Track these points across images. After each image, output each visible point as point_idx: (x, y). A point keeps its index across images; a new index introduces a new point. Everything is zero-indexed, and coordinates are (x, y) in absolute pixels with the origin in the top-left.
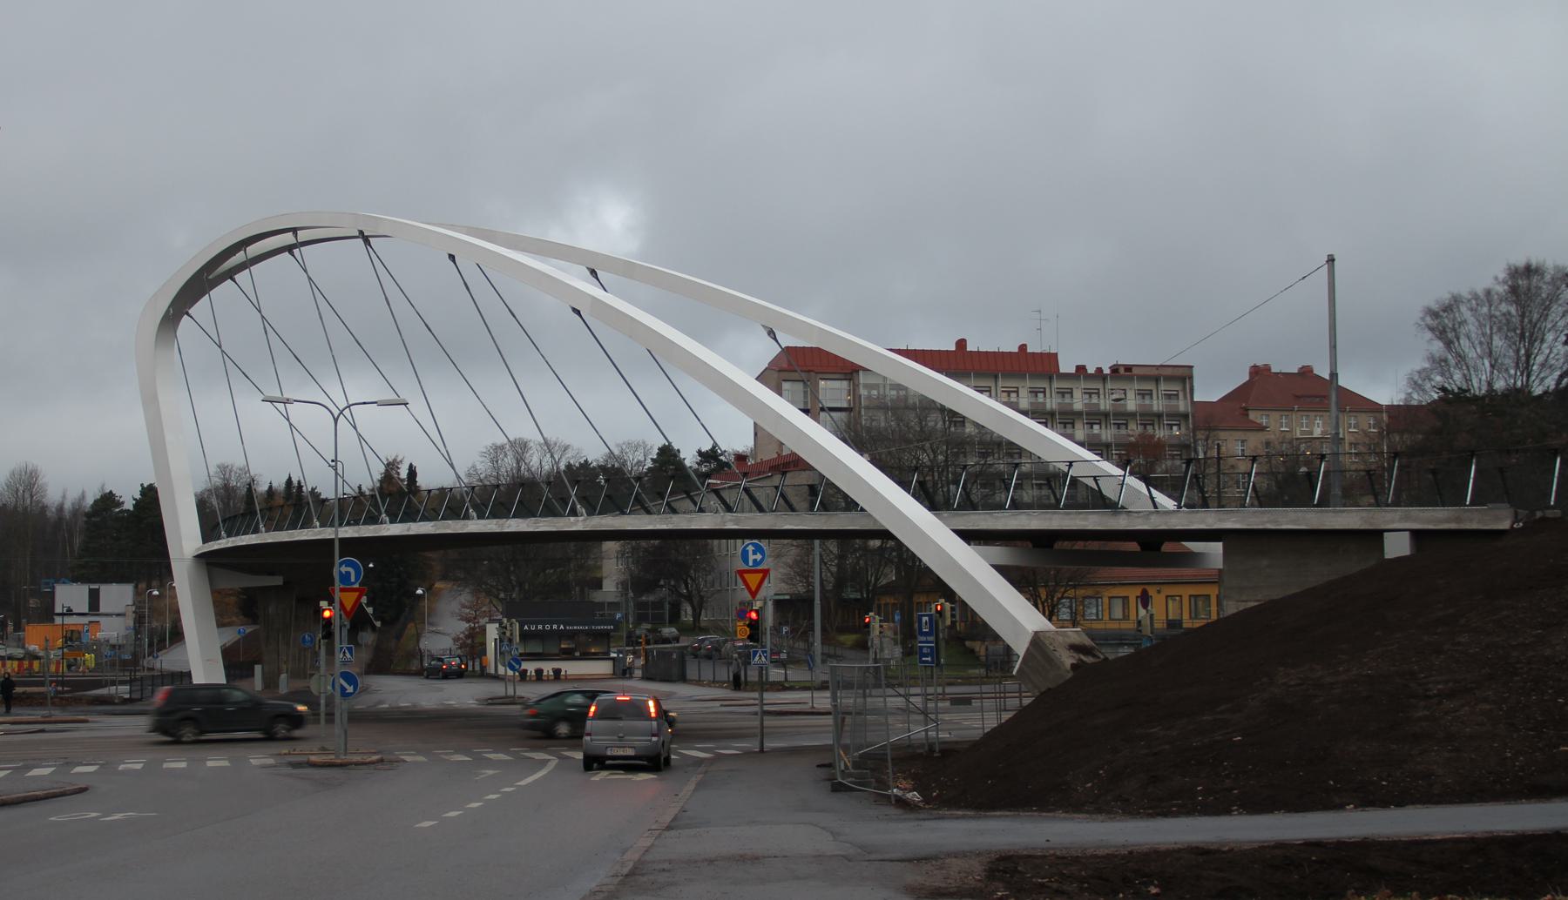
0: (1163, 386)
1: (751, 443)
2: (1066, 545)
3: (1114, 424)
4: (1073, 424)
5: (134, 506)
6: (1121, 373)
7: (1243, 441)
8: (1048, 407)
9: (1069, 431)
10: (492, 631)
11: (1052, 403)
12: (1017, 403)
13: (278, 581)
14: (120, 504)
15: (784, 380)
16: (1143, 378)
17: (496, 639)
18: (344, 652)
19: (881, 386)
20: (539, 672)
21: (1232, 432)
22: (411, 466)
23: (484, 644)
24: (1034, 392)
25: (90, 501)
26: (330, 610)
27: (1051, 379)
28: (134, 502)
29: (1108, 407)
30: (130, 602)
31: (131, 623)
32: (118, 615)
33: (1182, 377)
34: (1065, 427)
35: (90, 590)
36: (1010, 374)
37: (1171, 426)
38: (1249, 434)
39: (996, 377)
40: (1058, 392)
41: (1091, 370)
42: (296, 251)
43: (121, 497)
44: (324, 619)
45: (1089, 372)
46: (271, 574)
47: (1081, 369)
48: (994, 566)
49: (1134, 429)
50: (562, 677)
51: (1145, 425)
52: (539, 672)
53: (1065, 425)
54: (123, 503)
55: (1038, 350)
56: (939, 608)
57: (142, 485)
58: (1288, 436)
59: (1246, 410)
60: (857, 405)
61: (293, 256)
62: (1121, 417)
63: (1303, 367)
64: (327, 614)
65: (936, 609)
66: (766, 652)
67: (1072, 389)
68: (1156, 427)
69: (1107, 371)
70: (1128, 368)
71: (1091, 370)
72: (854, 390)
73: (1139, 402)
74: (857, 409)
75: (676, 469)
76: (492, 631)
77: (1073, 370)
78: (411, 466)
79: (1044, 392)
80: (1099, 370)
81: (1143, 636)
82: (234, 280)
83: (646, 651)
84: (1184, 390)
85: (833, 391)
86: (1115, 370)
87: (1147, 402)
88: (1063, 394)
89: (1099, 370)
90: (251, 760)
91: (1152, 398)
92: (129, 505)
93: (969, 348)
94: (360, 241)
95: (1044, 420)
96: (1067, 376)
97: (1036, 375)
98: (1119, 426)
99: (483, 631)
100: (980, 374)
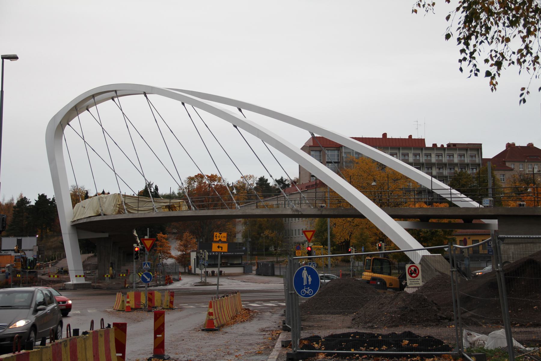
0: (469, 152)
1: (298, 176)
2: (434, 221)
3: (449, 168)
4: (431, 168)
5: (36, 204)
6: (452, 147)
7: (503, 175)
8: (421, 161)
9: (430, 171)
10: (193, 255)
11: (423, 159)
12: (408, 160)
13: (106, 235)
14: (29, 203)
15: (312, 151)
16: (460, 149)
17: (195, 259)
18: (146, 265)
19: (352, 153)
20: (213, 272)
21: (499, 171)
22: (156, 186)
23: (189, 261)
24: (415, 155)
25: (15, 202)
26: (138, 248)
27: (422, 149)
28: (35, 202)
29: (446, 161)
30: (35, 244)
31: (36, 254)
32: (30, 250)
33: (477, 148)
34: (428, 169)
35: (18, 240)
36: (405, 148)
37: (473, 169)
38: (506, 172)
39: (399, 149)
40: (425, 155)
41: (439, 146)
42: (116, 99)
43: (29, 200)
44: (135, 251)
45: (438, 146)
46: (103, 232)
47: (435, 145)
48: (406, 229)
49: (458, 170)
50: (215, 275)
51: (462, 168)
52: (213, 272)
53: (428, 168)
54: (30, 202)
55: (417, 138)
56: (380, 245)
57: (39, 194)
58: (523, 172)
59: (505, 162)
60: (342, 160)
61: (114, 101)
62: (452, 165)
63: (529, 144)
64: (137, 249)
65: (379, 246)
66: (314, 263)
67: (431, 154)
68: (466, 169)
69: (445, 146)
70: (454, 145)
71: (439, 146)
72: (340, 154)
73: (459, 159)
74: (342, 162)
75: (266, 187)
76: (193, 255)
77: (431, 146)
78: (156, 186)
79: (419, 155)
80: (442, 146)
81: (465, 257)
82: (88, 111)
83: (257, 263)
84: (478, 154)
85: (332, 155)
86: (449, 145)
87: (463, 158)
88: (427, 156)
89: (442, 146)
90: (88, 311)
91: (464, 157)
92: (33, 203)
93: (388, 137)
94: (143, 95)
95: (419, 167)
96: (429, 148)
97: (416, 148)
98: (451, 169)
99: (189, 254)
100: (392, 148)
